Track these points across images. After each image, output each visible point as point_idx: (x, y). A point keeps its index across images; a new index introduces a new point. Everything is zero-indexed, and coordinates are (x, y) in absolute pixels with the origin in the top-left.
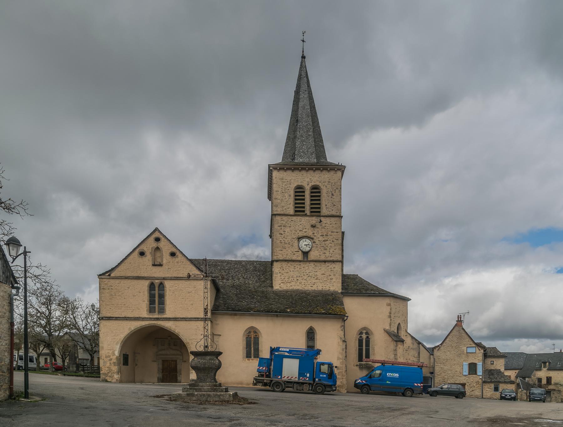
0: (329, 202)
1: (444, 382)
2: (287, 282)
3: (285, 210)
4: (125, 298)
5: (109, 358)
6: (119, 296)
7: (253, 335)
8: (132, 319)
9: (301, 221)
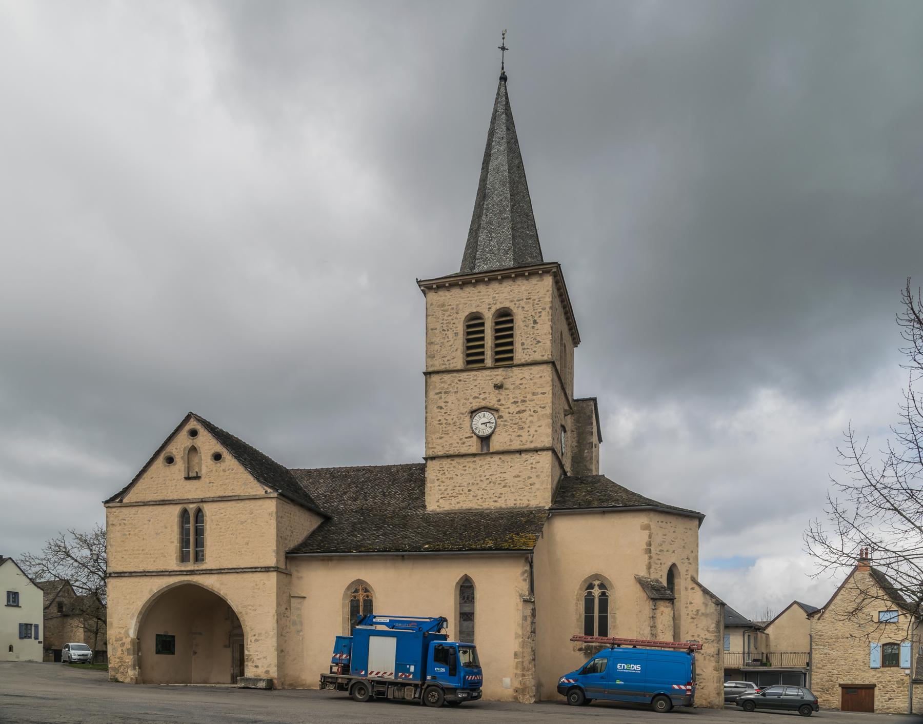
0: (528, 337)
1: (831, 681)
2: (451, 497)
3: (447, 363)
4: (144, 539)
5: (121, 642)
6: (135, 535)
7: (361, 597)
8: (154, 574)
9: (476, 380)
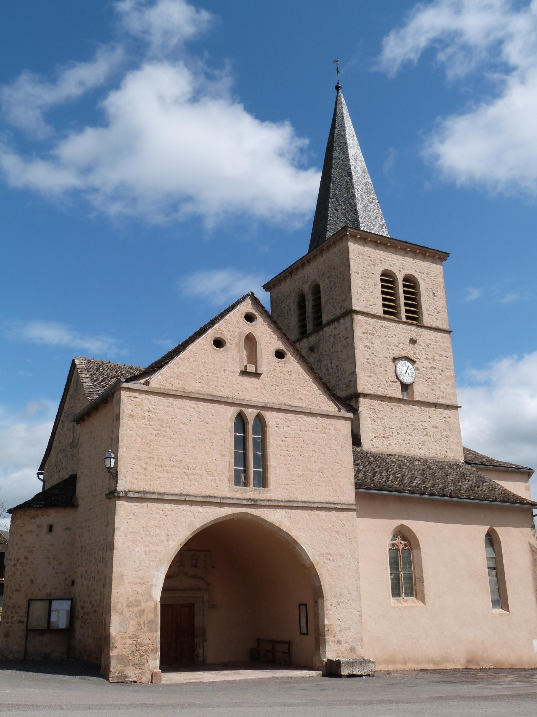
5: (136, 609)
